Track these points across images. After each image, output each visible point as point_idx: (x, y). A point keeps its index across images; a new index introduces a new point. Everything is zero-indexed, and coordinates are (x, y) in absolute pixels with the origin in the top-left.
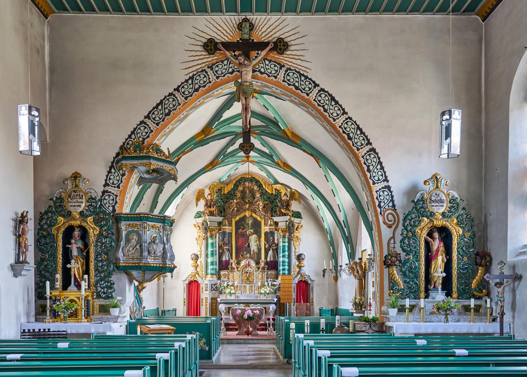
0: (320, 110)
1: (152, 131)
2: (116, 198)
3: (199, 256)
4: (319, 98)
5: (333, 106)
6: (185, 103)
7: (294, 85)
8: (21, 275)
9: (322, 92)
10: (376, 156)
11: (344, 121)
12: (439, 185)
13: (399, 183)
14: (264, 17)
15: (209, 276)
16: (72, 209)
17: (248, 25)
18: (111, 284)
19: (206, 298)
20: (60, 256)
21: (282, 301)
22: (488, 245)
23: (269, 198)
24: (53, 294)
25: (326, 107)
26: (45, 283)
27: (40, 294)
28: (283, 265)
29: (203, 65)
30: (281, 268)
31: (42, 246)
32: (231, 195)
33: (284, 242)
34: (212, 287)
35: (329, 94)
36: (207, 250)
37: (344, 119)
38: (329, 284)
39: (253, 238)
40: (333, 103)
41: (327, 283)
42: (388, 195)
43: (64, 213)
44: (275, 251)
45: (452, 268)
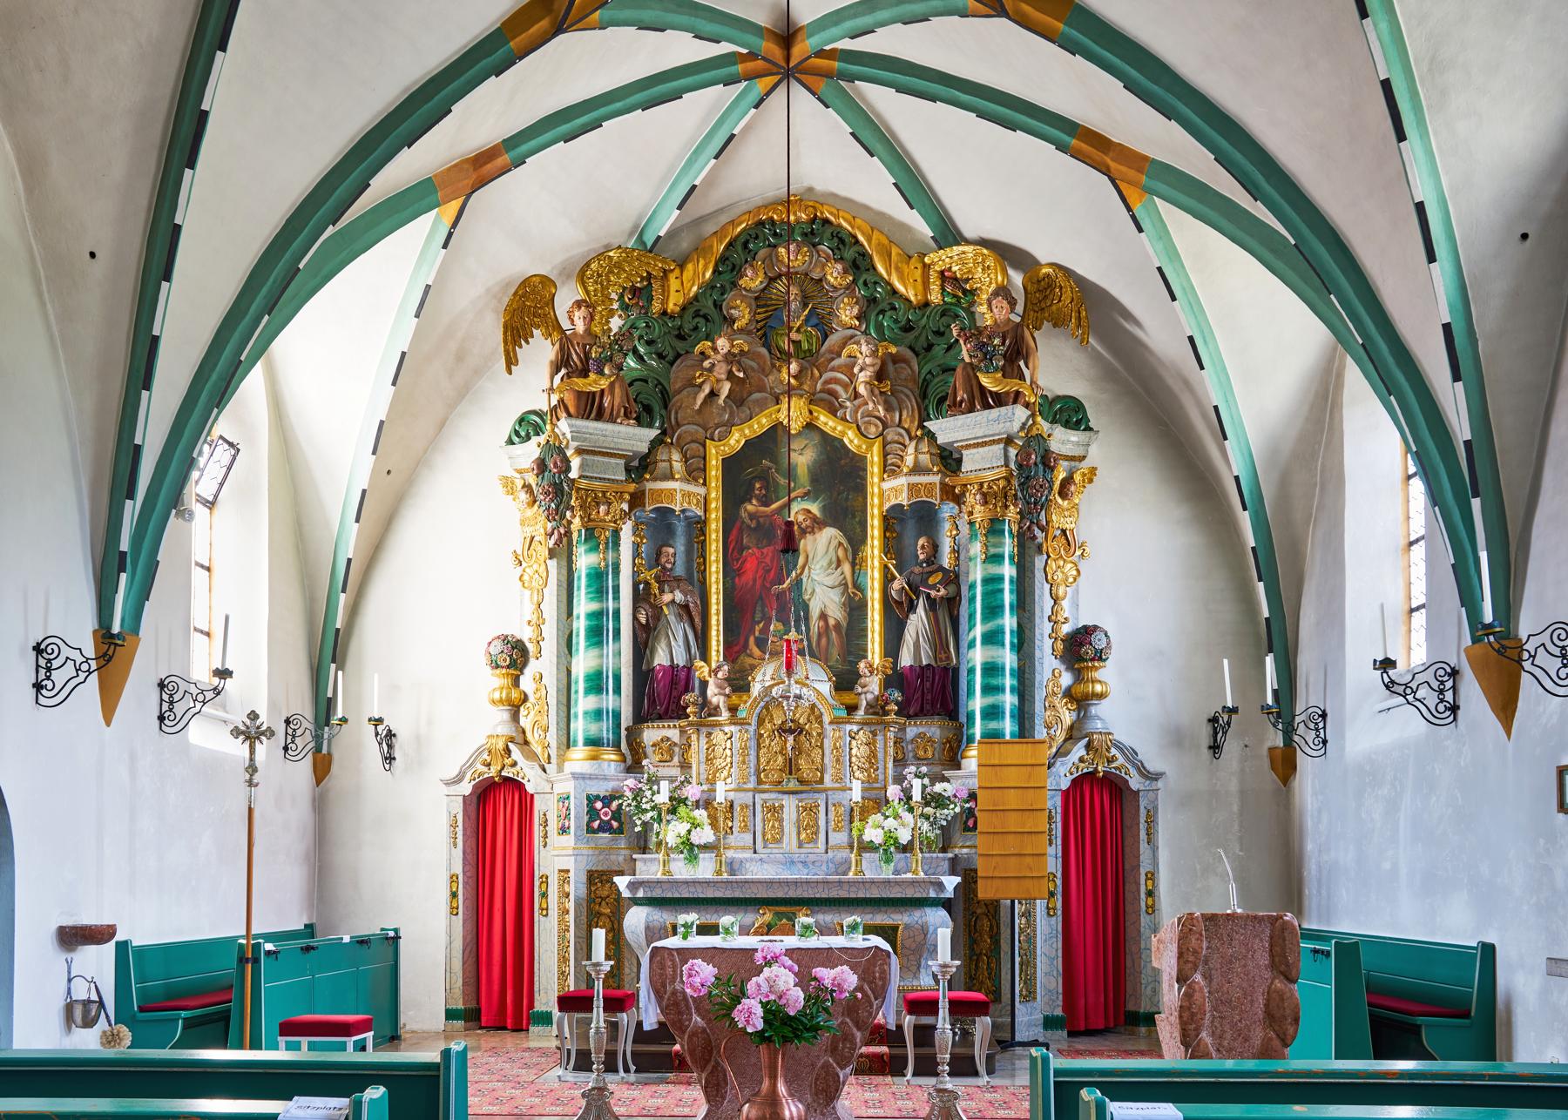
3: (531, 647)
15: (579, 752)
21: (984, 892)
23: (908, 328)
28: (988, 689)
30: (977, 703)
32: (704, 315)
34: (593, 813)
36: (570, 614)
38: (1243, 793)
39: (821, 546)
41: (1234, 786)
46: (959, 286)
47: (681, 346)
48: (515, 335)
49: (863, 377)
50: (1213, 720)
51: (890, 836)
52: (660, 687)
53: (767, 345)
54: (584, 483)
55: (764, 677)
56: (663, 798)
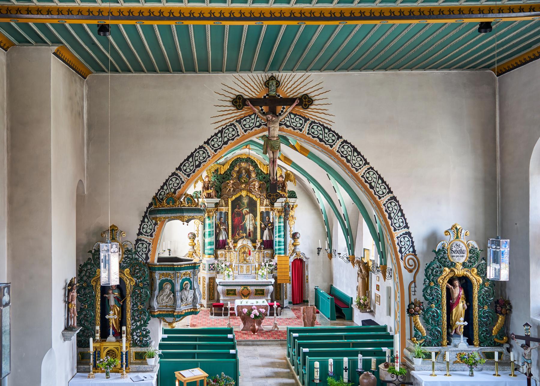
0: (343, 161)
1: (183, 182)
4: (342, 150)
5: (355, 157)
6: (214, 156)
7: (318, 137)
9: (344, 144)
11: (366, 171)
12: (459, 235)
13: (419, 230)
14: (289, 74)
15: (207, 256)
17: (275, 83)
18: (147, 333)
19: (204, 278)
20: (98, 306)
21: (279, 282)
22: (507, 291)
23: (264, 178)
25: (347, 158)
29: (232, 120)
32: (227, 176)
33: (280, 222)
34: (210, 267)
35: (351, 145)
36: (204, 229)
37: (366, 169)
38: (323, 261)
39: (249, 218)
40: (356, 154)
41: (322, 260)
42: (409, 241)
44: (271, 231)
45: (472, 315)
47: (224, 180)
50: (318, 249)
53: (239, 180)
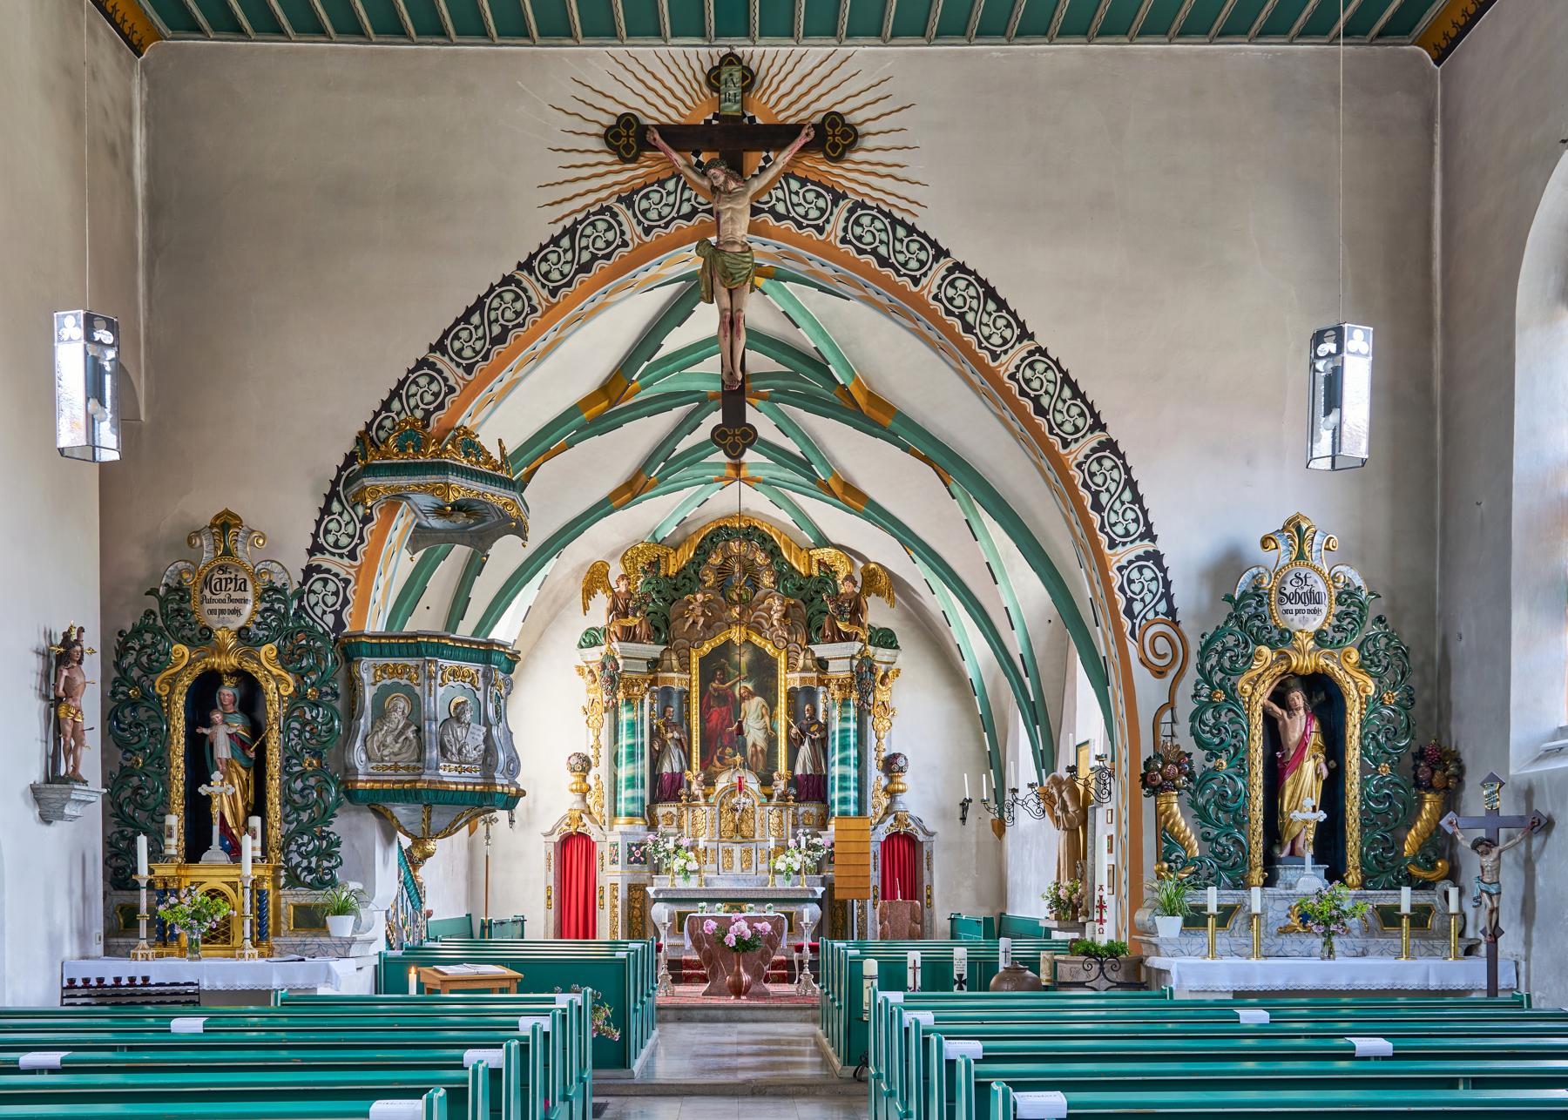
0: (952, 327)
1: (452, 390)
2: (345, 589)
3: (593, 760)
4: (951, 292)
5: (990, 314)
6: (551, 307)
7: (874, 252)
8: (62, 817)
9: (957, 274)
10: (1119, 462)
11: (1023, 360)
12: (1307, 549)
13: (1187, 544)
14: (785, 50)
15: (622, 820)
16: (213, 621)
17: (737, 76)
18: (331, 844)
19: (614, 886)
20: (178, 761)
21: (838, 895)
22: (1453, 727)
23: (800, 588)
24: (158, 872)
25: (969, 319)
26: (133, 841)
27: (119, 874)
28: (842, 789)
29: (604, 194)
30: (836, 796)
31: (124, 730)
32: (688, 579)
33: (846, 719)
34: (631, 853)
35: (978, 279)
36: (616, 742)
37: (1024, 354)
38: (978, 843)
39: (753, 708)
40: (991, 306)
41: (973, 840)
42: (1156, 578)
43: (190, 634)
44: (818, 747)
45: (1344, 795)
46: (827, 569)
48: (588, 593)
49: (776, 616)
51: (789, 867)
52: (666, 783)
54: (626, 675)
55: (722, 782)
56: (670, 846)
